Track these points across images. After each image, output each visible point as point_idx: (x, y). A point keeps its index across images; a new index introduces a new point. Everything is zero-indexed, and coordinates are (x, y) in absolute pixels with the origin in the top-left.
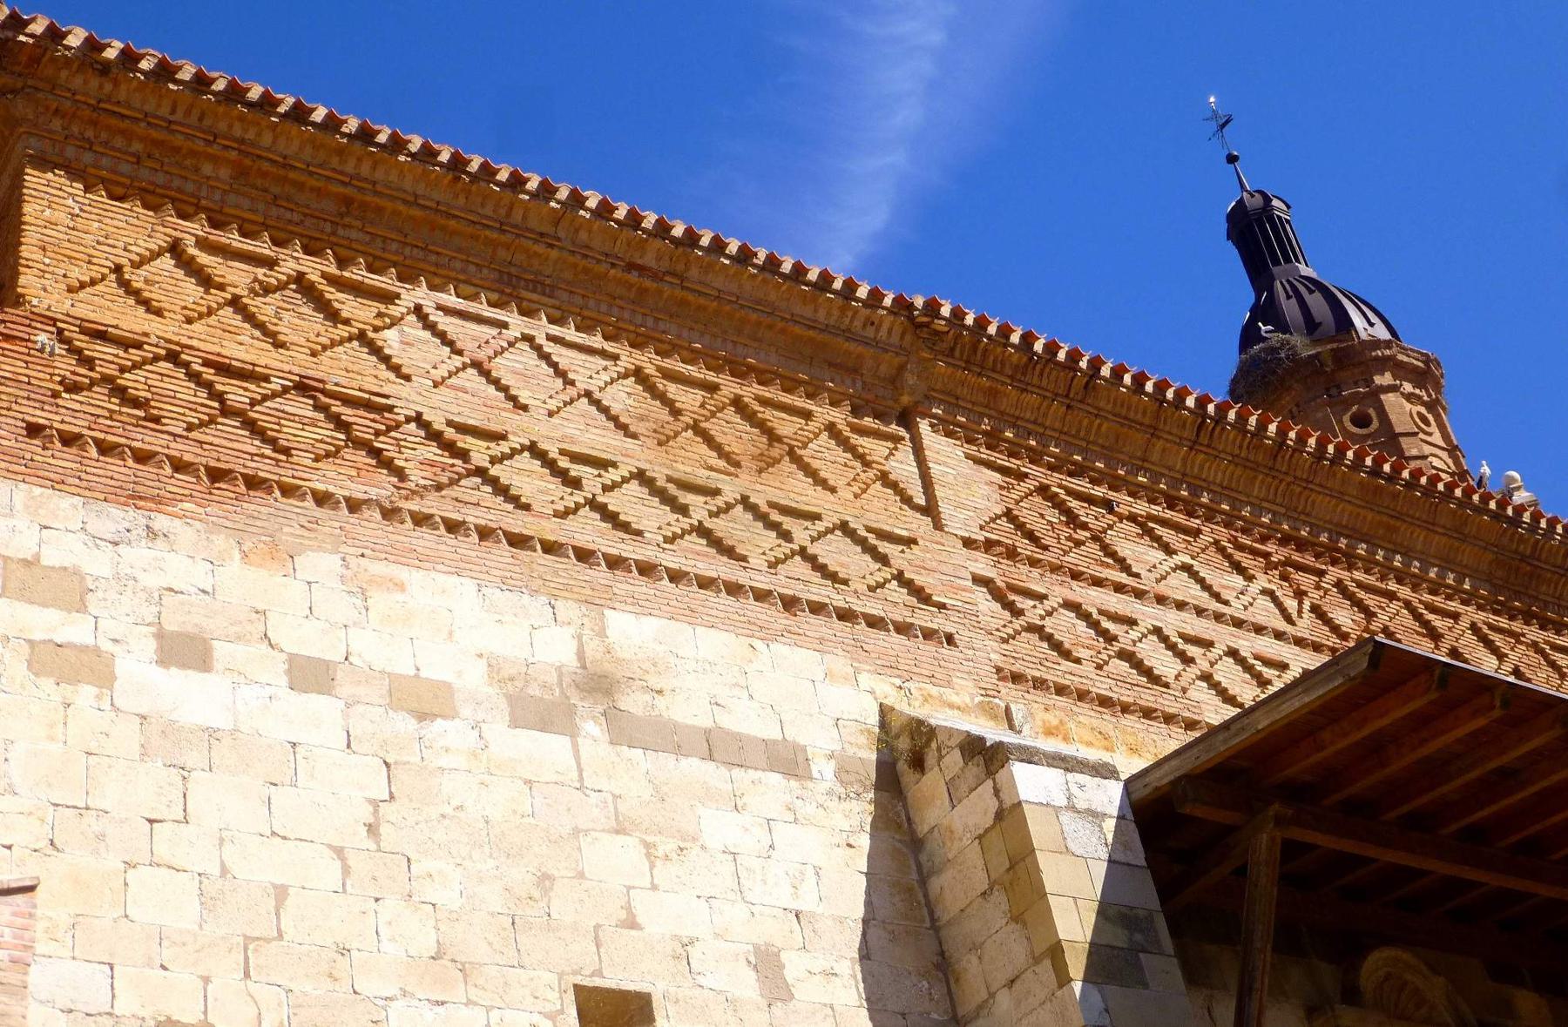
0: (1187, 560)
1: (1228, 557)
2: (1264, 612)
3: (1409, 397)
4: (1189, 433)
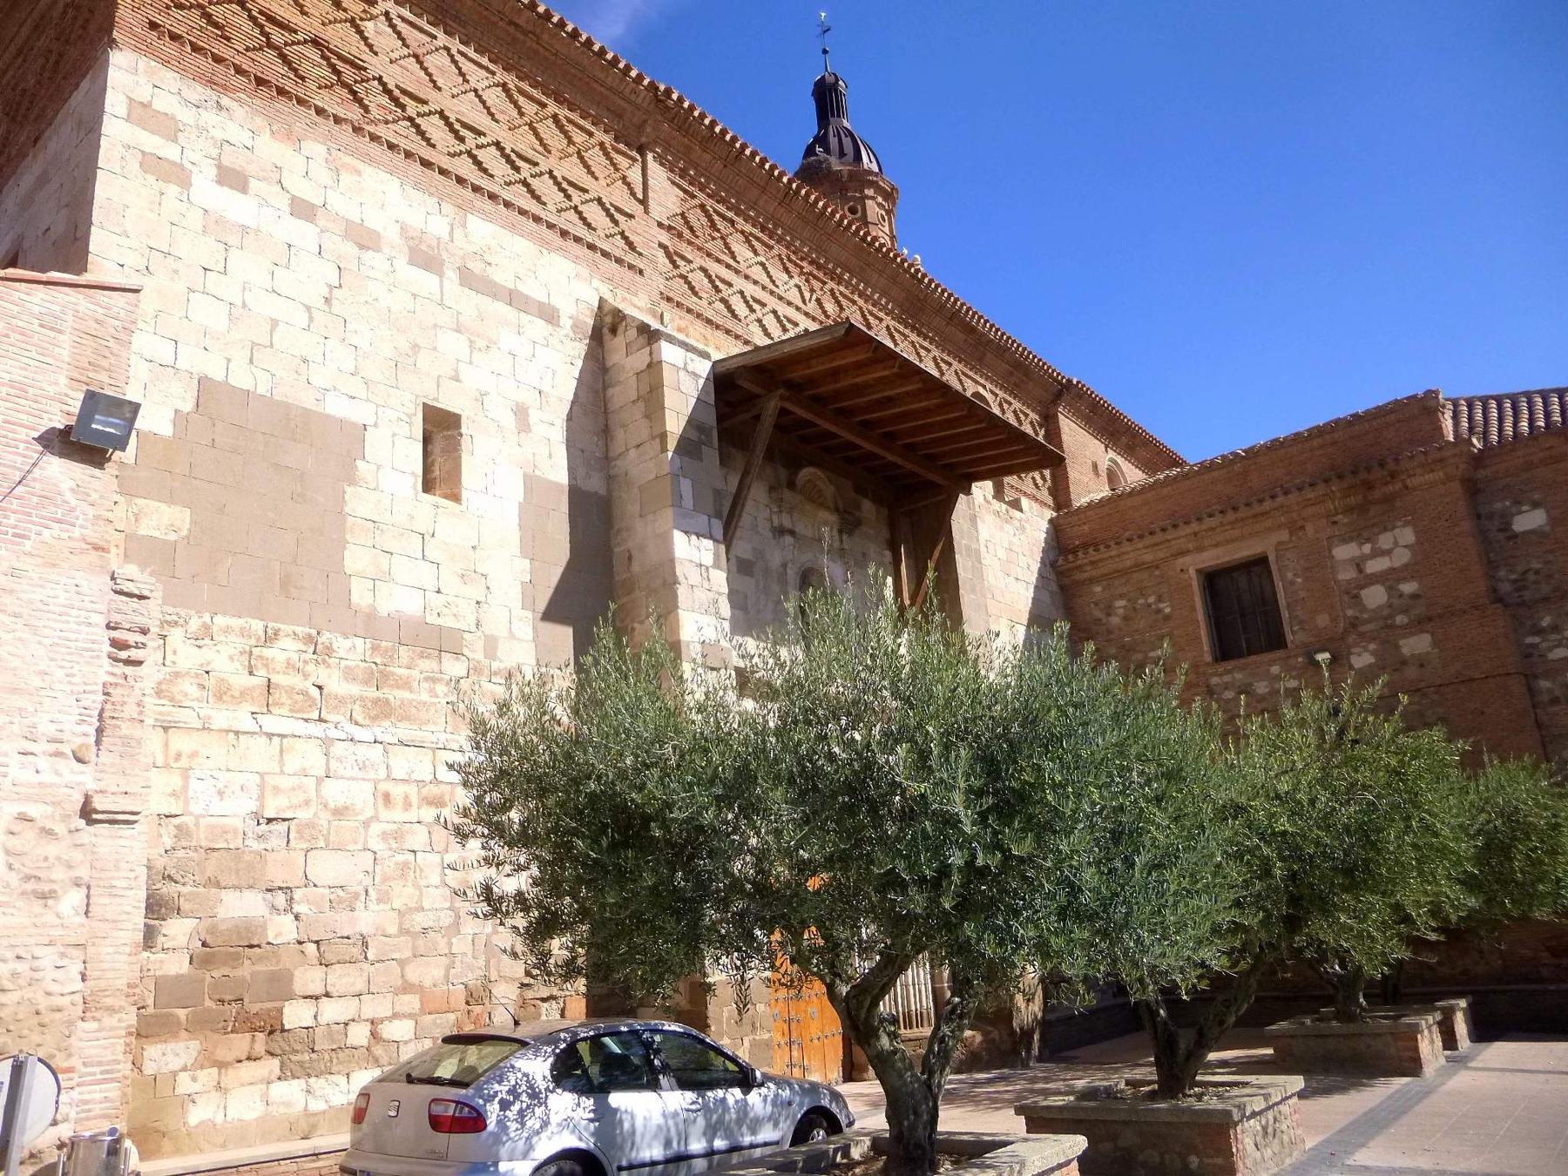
0: (764, 260)
1: (784, 264)
2: (794, 296)
3: (880, 205)
4: (781, 196)
